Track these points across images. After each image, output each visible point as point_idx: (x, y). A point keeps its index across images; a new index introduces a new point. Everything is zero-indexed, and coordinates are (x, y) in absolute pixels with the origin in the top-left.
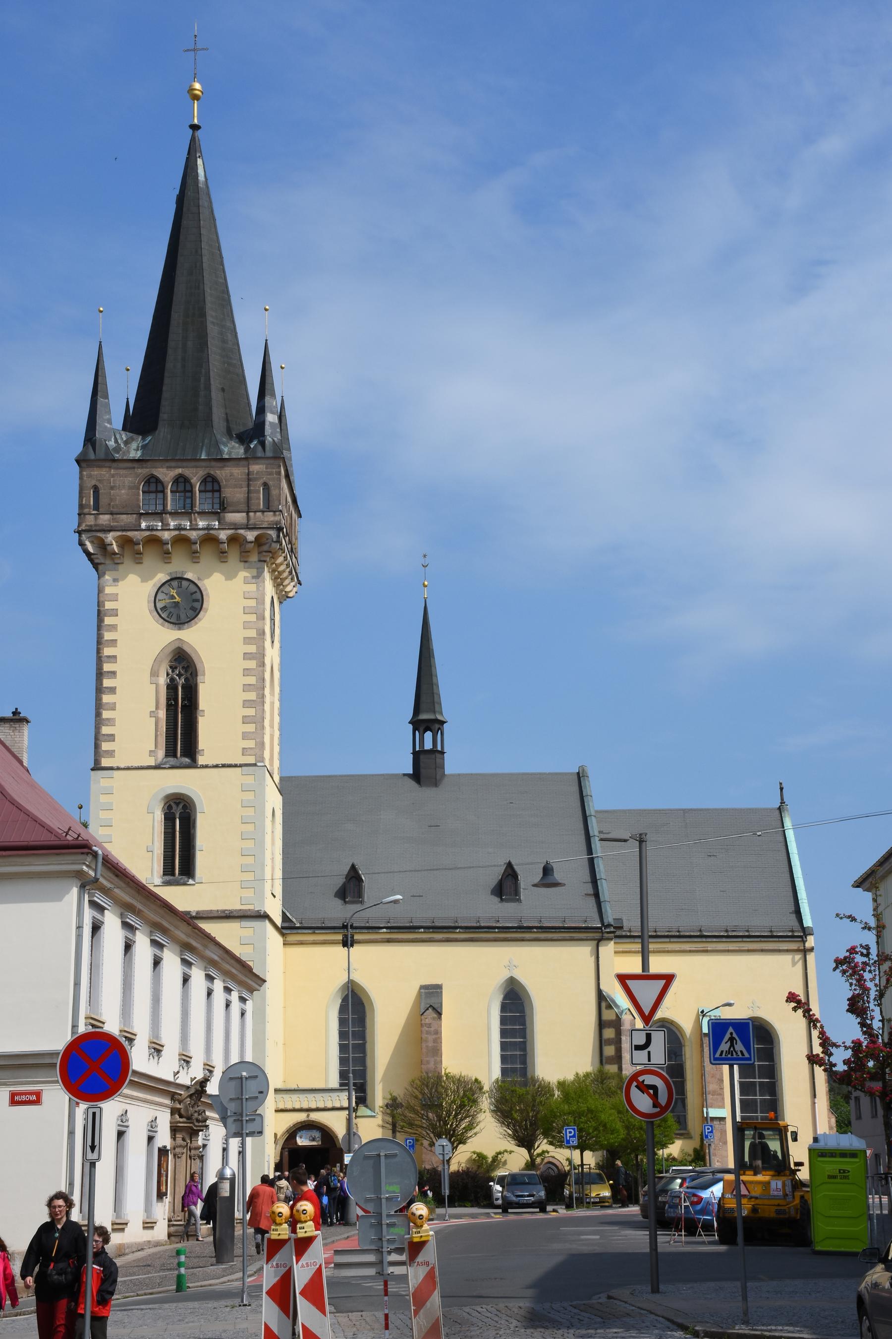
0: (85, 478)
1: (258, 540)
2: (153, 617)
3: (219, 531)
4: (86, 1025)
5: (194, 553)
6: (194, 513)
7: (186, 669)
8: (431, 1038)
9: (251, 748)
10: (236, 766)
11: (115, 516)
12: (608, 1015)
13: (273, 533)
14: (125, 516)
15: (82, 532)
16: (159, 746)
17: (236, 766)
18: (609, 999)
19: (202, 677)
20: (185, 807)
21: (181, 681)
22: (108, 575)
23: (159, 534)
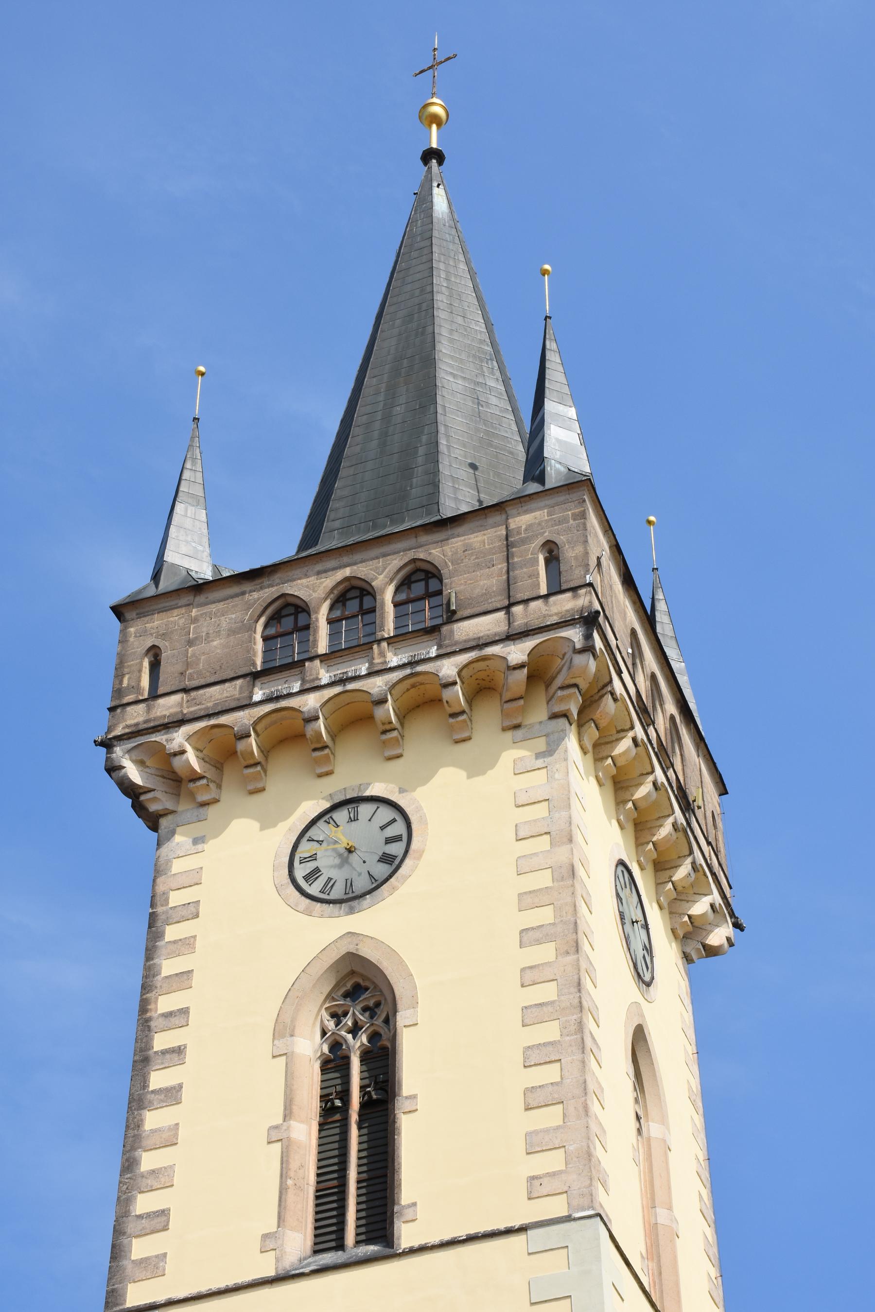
0: (132, 639)
3: (438, 663)
5: (384, 732)
6: (379, 642)
7: (371, 1011)
10: (509, 1232)
11: (193, 694)
13: (575, 635)
16: (290, 1219)
19: (409, 1012)
21: (356, 1044)
22: (183, 834)
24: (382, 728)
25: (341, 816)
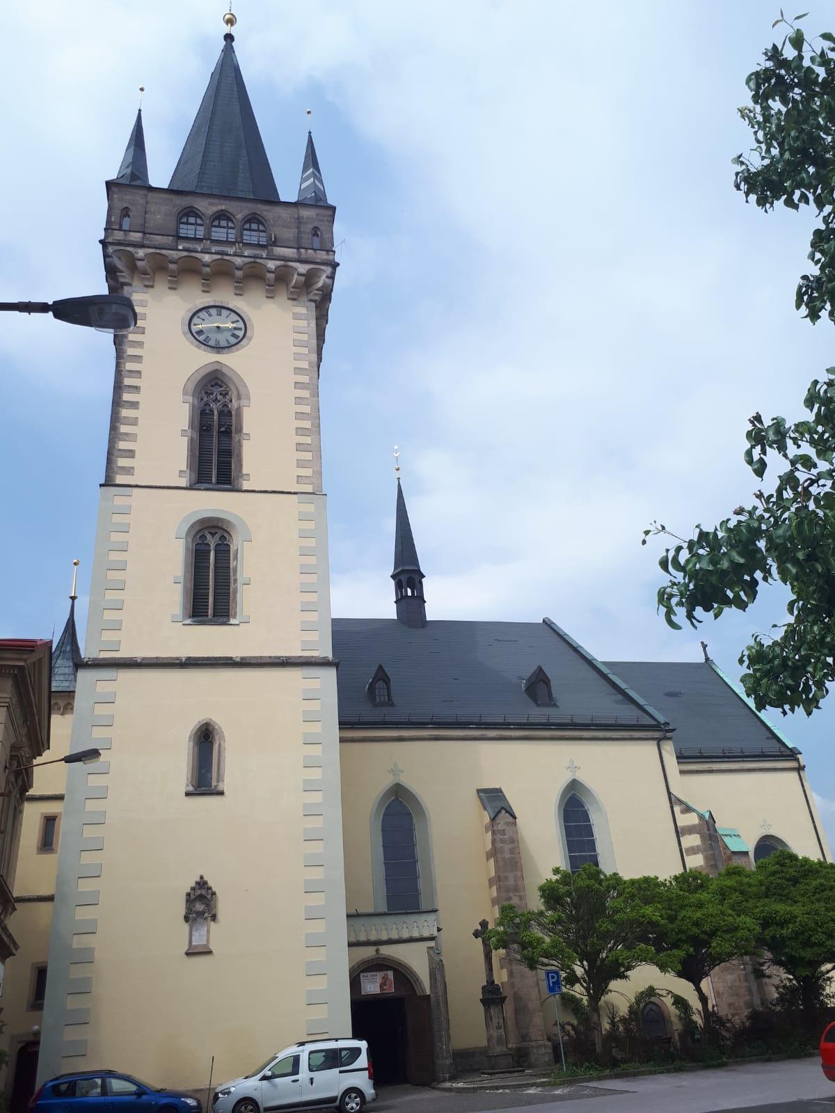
2: (188, 339)
3: (266, 261)
4: (71, 694)
8: (507, 847)
14: (160, 237)
15: (108, 244)
23: (199, 255)
24: (236, 280)
25: (213, 311)
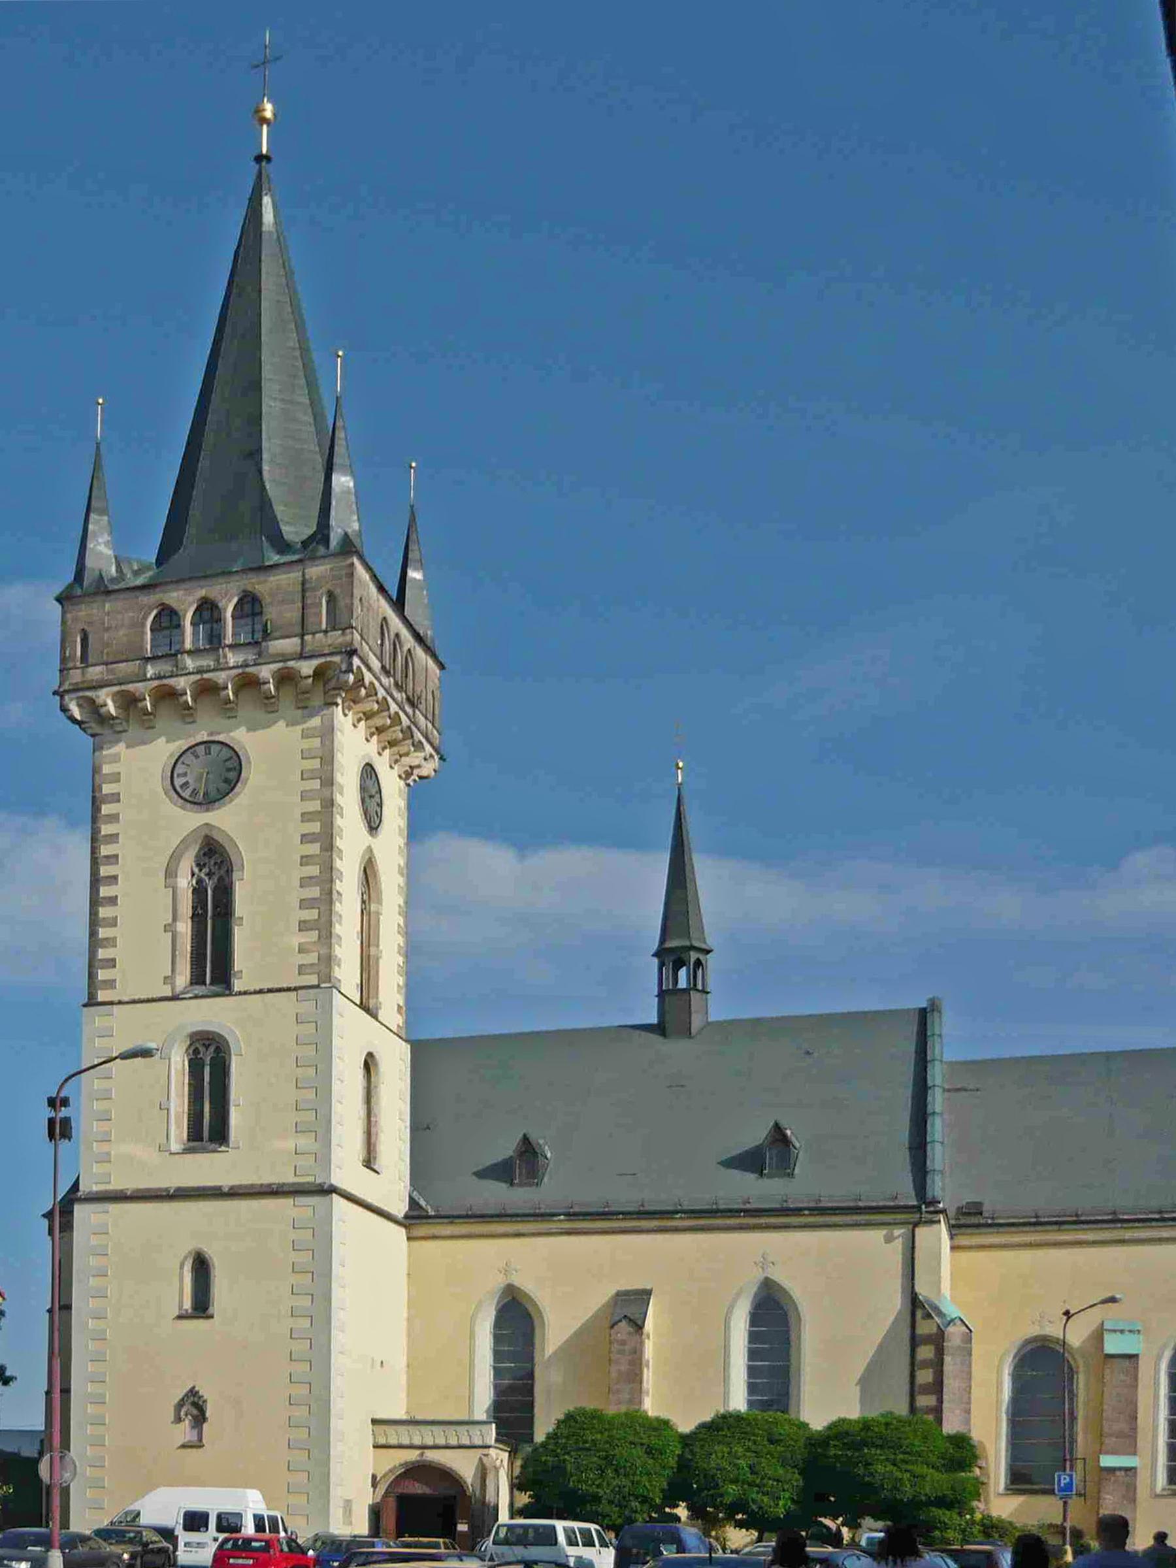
1: (318, 673)
3: (259, 667)
5: (226, 704)
6: (223, 648)
7: (219, 865)
9: (312, 965)
10: (289, 989)
11: (110, 667)
12: (925, 1328)
17: (289, 989)
18: (928, 1305)
20: (218, 1050)
